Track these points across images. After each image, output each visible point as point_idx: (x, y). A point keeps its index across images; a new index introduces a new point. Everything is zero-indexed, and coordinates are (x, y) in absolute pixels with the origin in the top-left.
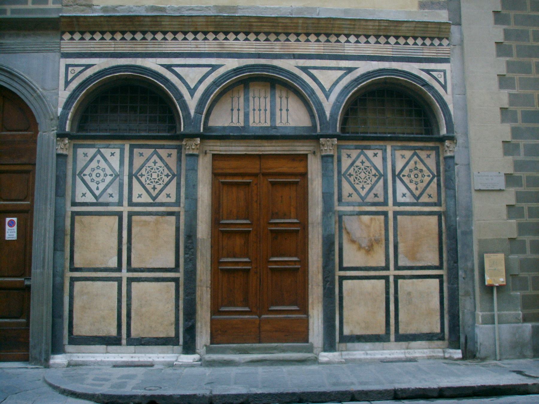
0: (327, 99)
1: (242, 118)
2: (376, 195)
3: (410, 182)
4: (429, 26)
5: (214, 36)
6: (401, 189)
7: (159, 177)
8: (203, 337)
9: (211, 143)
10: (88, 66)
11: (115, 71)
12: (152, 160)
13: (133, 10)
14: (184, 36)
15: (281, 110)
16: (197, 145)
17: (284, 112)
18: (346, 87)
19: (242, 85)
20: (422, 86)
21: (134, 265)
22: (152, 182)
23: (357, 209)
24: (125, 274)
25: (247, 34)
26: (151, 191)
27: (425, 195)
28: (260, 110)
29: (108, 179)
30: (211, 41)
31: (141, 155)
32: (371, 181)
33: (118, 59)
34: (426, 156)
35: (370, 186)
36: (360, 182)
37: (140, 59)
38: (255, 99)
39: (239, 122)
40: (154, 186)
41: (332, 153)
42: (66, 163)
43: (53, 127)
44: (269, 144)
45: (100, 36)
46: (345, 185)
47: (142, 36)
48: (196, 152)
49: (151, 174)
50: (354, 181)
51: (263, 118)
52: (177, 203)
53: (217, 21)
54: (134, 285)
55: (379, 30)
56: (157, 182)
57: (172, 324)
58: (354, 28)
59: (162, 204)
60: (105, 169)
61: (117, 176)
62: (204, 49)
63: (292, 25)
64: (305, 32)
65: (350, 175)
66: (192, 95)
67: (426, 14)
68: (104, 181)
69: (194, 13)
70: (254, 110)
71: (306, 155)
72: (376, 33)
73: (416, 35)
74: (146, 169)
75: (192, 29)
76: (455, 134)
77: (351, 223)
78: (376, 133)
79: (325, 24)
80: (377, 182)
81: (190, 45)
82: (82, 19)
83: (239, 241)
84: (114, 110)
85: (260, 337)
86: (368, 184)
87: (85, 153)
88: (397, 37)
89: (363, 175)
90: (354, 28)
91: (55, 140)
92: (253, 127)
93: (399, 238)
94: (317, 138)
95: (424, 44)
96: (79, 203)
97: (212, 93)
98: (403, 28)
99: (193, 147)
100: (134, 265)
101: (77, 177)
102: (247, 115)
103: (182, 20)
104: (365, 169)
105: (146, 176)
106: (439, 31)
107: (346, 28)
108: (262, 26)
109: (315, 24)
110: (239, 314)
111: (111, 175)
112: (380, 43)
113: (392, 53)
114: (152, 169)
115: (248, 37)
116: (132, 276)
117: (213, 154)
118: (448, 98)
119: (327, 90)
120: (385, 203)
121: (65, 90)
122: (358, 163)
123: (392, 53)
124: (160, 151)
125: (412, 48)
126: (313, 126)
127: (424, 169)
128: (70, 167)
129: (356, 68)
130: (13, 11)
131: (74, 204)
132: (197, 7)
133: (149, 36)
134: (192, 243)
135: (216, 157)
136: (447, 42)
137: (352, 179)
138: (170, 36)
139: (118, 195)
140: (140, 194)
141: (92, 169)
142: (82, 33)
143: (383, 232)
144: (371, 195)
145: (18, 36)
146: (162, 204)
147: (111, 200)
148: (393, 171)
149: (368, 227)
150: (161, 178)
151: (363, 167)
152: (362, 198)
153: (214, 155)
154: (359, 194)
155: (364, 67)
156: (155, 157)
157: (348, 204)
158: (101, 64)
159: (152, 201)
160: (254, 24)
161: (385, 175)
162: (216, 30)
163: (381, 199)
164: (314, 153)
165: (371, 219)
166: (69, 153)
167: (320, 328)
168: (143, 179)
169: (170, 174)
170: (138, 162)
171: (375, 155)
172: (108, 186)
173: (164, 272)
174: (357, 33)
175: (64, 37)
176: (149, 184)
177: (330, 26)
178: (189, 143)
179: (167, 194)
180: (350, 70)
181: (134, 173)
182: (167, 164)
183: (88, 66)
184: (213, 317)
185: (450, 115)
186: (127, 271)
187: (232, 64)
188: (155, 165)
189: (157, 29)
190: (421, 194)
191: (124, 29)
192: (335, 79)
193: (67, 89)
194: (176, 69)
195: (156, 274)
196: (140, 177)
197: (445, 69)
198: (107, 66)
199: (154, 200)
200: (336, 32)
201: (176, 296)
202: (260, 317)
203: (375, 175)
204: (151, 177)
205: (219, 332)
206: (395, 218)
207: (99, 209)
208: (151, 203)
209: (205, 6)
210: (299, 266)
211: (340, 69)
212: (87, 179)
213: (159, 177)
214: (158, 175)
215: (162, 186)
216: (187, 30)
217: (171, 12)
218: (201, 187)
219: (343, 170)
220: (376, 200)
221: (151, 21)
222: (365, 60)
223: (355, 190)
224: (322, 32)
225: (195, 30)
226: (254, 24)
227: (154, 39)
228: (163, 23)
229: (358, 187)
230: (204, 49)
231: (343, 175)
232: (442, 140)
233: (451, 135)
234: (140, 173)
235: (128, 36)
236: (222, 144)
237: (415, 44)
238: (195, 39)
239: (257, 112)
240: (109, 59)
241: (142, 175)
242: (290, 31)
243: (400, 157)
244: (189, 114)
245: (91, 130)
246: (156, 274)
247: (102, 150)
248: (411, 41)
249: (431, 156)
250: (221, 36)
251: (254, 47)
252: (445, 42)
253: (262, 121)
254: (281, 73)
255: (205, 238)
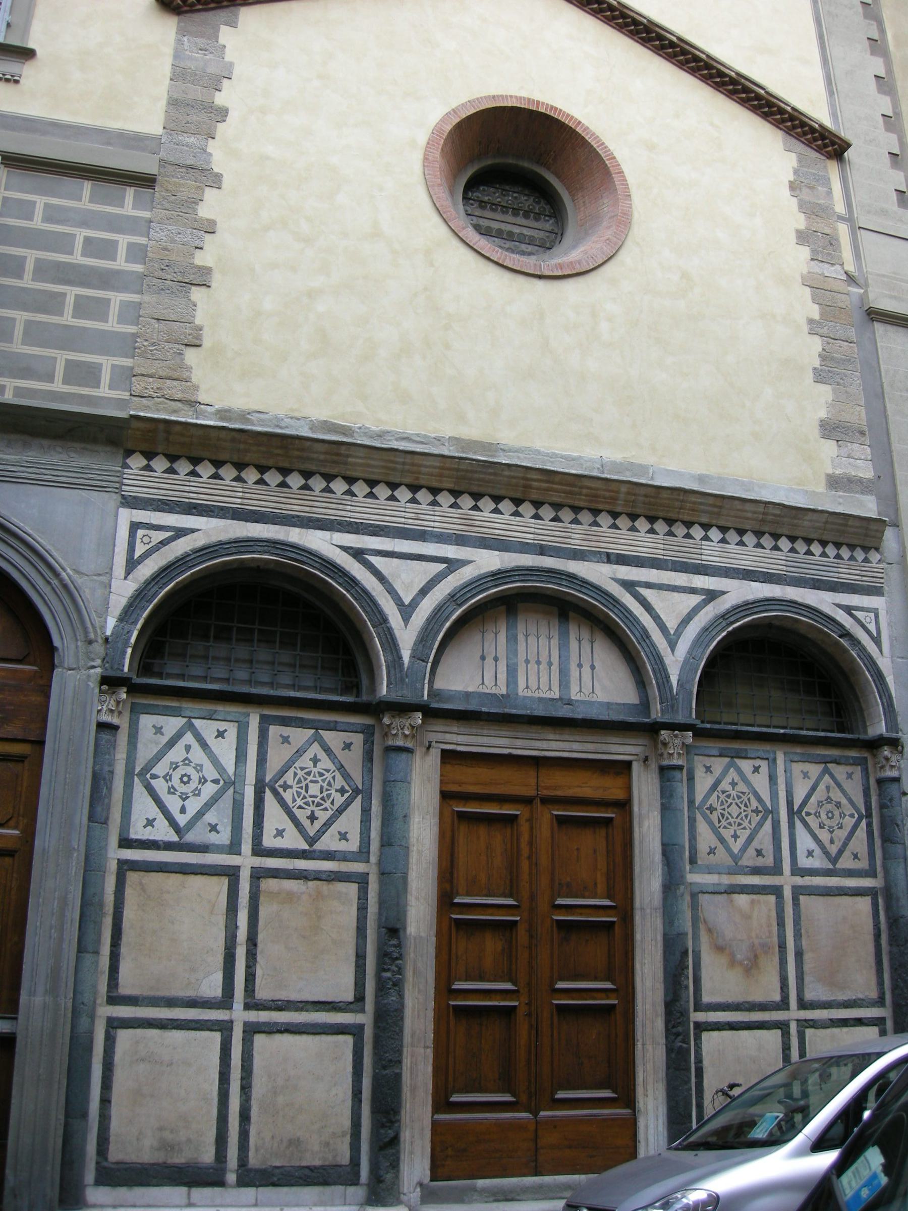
0: (673, 651)
1: (502, 677)
2: (759, 853)
3: (821, 827)
4: (850, 523)
5: (453, 500)
6: (804, 841)
7: (325, 794)
8: (415, 1165)
9: (439, 726)
10: (181, 532)
11: (242, 549)
12: (310, 754)
13: (283, 424)
14: (390, 492)
15: (580, 666)
16: (413, 727)
17: (586, 669)
18: (705, 630)
19: (503, 608)
20: (840, 636)
21: (263, 993)
22: (307, 804)
23: (726, 880)
24: (239, 1015)
25: (517, 502)
26: (306, 823)
27: (847, 853)
28: (538, 663)
29: (209, 790)
30: (445, 508)
31: (286, 740)
32: (750, 822)
33: (248, 524)
34: (845, 776)
35: (748, 832)
36: (730, 824)
37: (297, 530)
38: (529, 638)
39: (496, 685)
40: (313, 812)
41: (680, 763)
42: (113, 745)
43: (93, 660)
44: (557, 737)
45: (212, 470)
46: (702, 827)
47: (303, 482)
48: (409, 744)
49: (307, 786)
50: (719, 821)
51: (544, 679)
52: (363, 854)
53: (463, 470)
54: (259, 1040)
55: (763, 521)
56: (319, 805)
57: (344, 1135)
58: (719, 514)
59: (329, 856)
60: (201, 766)
61: (229, 784)
62: (432, 524)
63: (607, 494)
64: (629, 510)
65: (712, 809)
66: (406, 618)
67: (841, 500)
68: (199, 795)
69: (419, 448)
70: (527, 661)
71: (628, 764)
72: (757, 528)
73: (824, 538)
74: (295, 774)
75: (407, 480)
76: (900, 734)
77: (715, 910)
78: (769, 727)
79: (669, 499)
80: (760, 824)
81: (402, 509)
82: (178, 428)
83: (491, 944)
84: (223, 635)
85: (536, 1161)
86: (744, 828)
87: (156, 727)
88: (793, 539)
89: (734, 810)
90: (719, 514)
91: (97, 690)
92: (525, 697)
93: (804, 943)
94: (652, 729)
95: (838, 556)
96: (137, 840)
97: (447, 619)
98: (806, 523)
99: (407, 732)
100: (263, 993)
101: (136, 778)
102: (512, 672)
103: (392, 458)
104: (739, 797)
105: (295, 789)
106: (866, 535)
107: (703, 512)
108: (547, 490)
109: (651, 497)
110: (491, 1110)
111: (216, 782)
112: (764, 548)
113: (785, 568)
114: (309, 774)
115: (520, 509)
116: (255, 1020)
117: (443, 751)
118: (884, 663)
119: (672, 632)
120: (776, 870)
121: (125, 578)
122: (725, 785)
123: (785, 568)
124: (326, 735)
125: (820, 560)
126: (641, 704)
127: (844, 801)
128: (121, 756)
129: (724, 593)
130: (18, 391)
131: (126, 843)
132: (418, 435)
133: (318, 484)
134: (399, 946)
135: (448, 756)
136: (878, 557)
137: (714, 817)
138: (360, 489)
139: (229, 828)
140: (279, 830)
141: (172, 763)
142: (172, 458)
143: (775, 928)
144: (751, 852)
145: (26, 446)
146: (329, 856)
147: (213, 838)
148: (790, 803)
149: (748, 917)
150: (329, 796)
151: (734, 793)
152: (736, 858)
153: (443, 751)
154: (728, 849)
155: (740, 592)
156: (316, 749)
157: (710, 870)
158: (210, 530)
159: (307, 847)
160: (535, 484)
161: (773, 812)
162: (456, 488)
163: (769, 861)
164: (646, 759)
165: (753, 902)
166: (123, 721)
167: (661, 1138)
168: (287, 796)
169: (347, 788)
170: (276, 757)
171: (756, 769)
172: (208, 806)
173: (328, 1011)
174: (722, 523)
175: (129, 461)
176: (300, 807)
177: (677, 504)
178: (397, 722)
179: (339, 833)
180: (712, 595)
181: (267, 779)
182: (342, 766)
183: (181, 532)
184: (436, 1117)
185: (890, 696)
186: (241, 1013)
187: (489, 561)
188: (315, 766)
189: (334, 471)
190: (840, 852)
191: (264, 462)
192: (685, 612)
193: (130, 577)
194: (374, 560)
195: (303, 1018)
196: (281, 790)
197: (876, 607)
198: (224, 537)
199: (311, 845)
200: (686, 518)
201: (354, 1067)
202: (536, 1114)
203: (756, 811)
204: (307, 791)
205: (450, 1152)
206: (796, 900)
207: (183, 857)
208: (304, 851)
209: (433, 435)
210: (616, 1002)
211: (693, 591)
212: (160, 786)
213: (325, 794)
214: (322, 787)
215: (330, 813)
216: (397, 480)
217: (364, 438)
218: (417, 820)
219: (699, 798)
220: (760, 862)
221: (326, 453)
222: (741, 582)
223: (722, 840)
224: (661, 514)
225: (416, 483)
226: (535, 484)
227: (328, 490)
228: (350, 459)
229: (727, 834)
230: (432, 524)
231: (698, 808)
232: (874, 745)
233: (894, 735)
234: (281, 782)
235: (273, 478)
236: (463, 730)
237: (824, 554)
238: (413, 501)
239: (533, 667)
240: (229, 522)
241: (286, 787)
242: (601, 507)
243: (799, 777)
244: (400, 658)
245: (169, 676)
246: (303, 1018)
247: (197, 723)
248: (816, 548)
249: (853, 776)
250: (466, 502)
251: (532, 530)
252: (874, 556)
253: (544, 686)
254: (583, 590)
255: (423, 934)
